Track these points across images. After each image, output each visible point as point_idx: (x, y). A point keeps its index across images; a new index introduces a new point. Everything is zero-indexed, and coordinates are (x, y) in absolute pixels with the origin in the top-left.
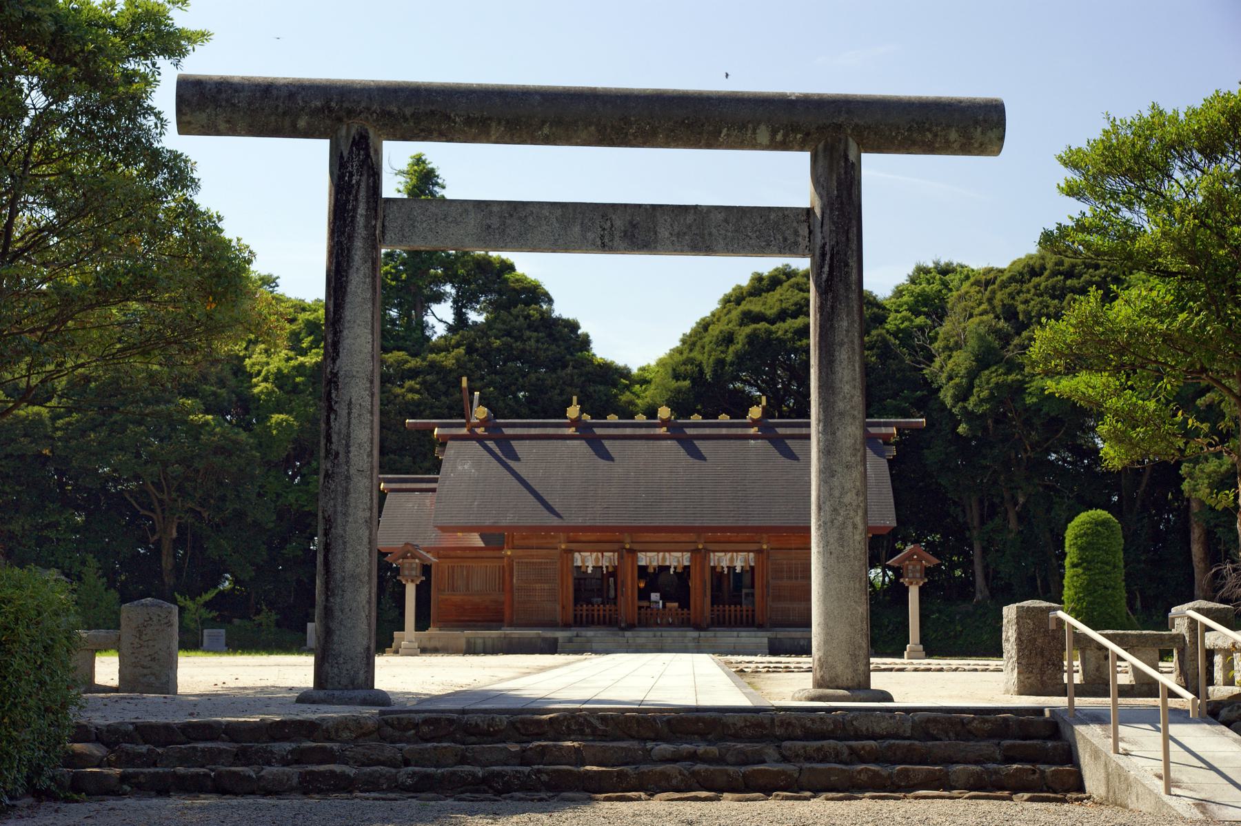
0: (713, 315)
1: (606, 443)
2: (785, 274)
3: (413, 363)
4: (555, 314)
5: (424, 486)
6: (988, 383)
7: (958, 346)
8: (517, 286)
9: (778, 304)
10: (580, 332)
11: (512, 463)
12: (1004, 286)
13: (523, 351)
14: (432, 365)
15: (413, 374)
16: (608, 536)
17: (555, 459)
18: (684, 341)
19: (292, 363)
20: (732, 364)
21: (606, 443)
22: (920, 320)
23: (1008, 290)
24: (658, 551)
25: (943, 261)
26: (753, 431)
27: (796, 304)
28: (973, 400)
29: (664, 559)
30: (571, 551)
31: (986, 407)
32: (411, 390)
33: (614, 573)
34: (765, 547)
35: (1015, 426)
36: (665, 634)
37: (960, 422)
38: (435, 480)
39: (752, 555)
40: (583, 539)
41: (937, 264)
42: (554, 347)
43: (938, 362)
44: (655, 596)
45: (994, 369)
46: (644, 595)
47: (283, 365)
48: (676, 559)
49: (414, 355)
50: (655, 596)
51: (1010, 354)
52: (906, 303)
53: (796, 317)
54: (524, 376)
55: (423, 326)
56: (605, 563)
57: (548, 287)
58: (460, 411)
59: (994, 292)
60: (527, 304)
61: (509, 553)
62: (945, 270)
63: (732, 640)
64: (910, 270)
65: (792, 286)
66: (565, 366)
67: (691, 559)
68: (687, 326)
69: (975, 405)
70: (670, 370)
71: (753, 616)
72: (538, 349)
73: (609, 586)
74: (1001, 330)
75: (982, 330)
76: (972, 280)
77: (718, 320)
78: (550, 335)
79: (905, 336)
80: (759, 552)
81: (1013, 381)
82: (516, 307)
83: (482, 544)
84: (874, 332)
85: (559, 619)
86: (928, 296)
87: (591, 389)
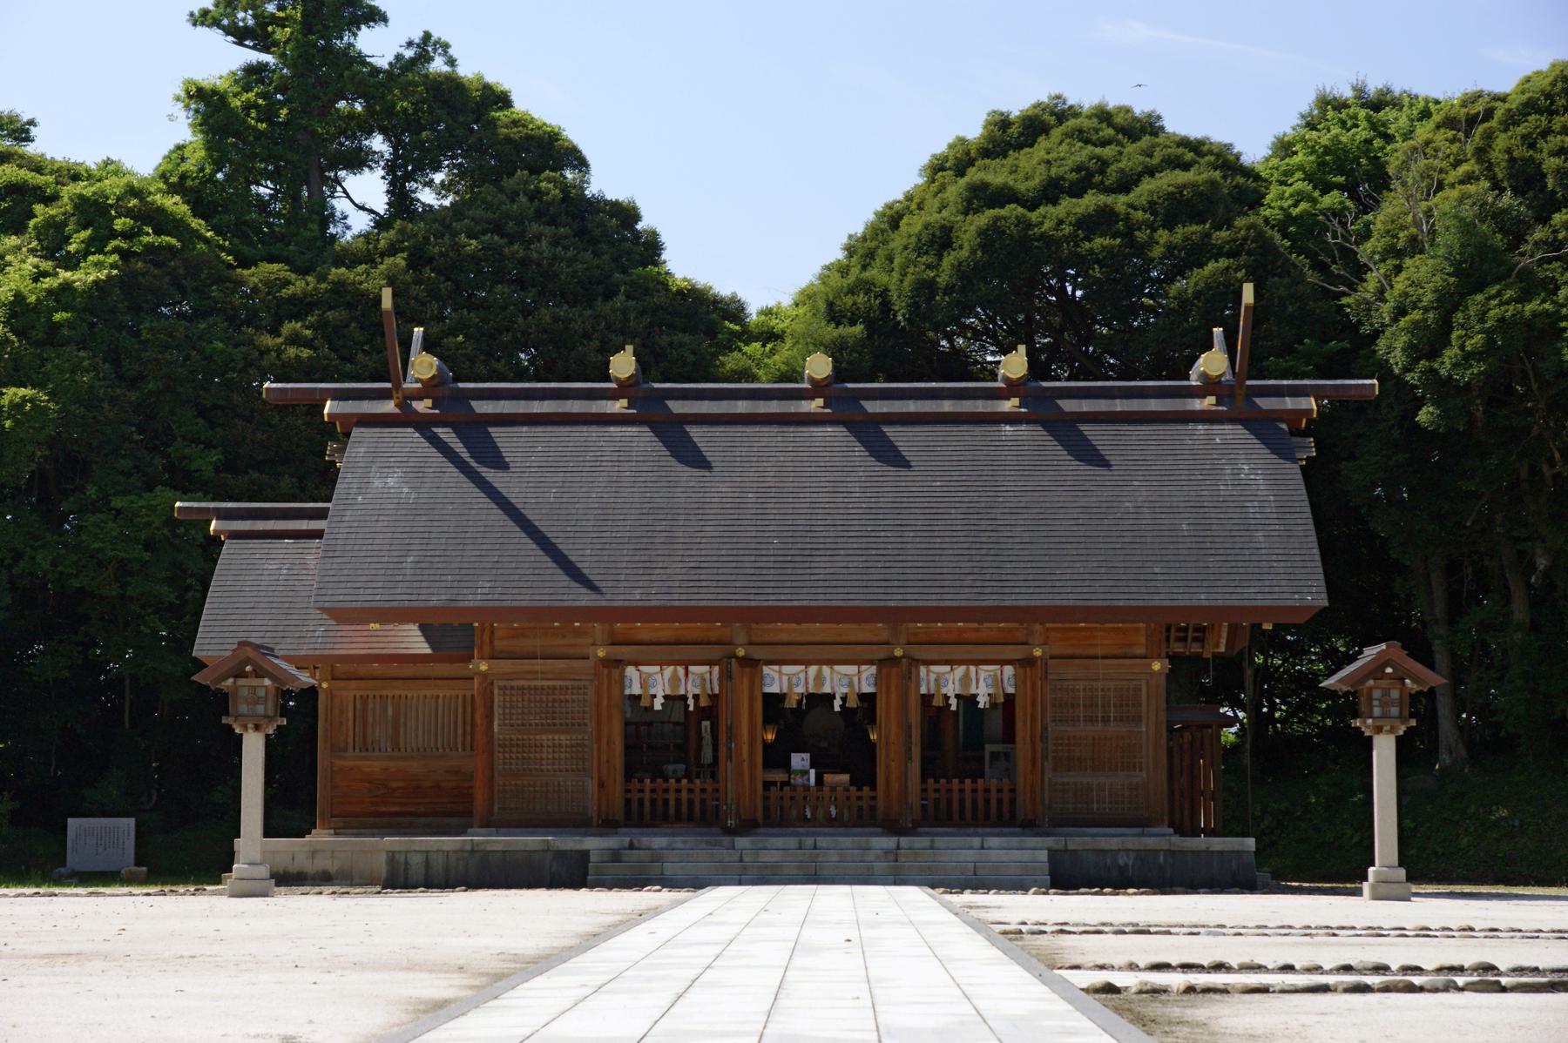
0: (909, 198)
1: (695, 432)
2: (1052, 113)
3: (299, 285)
4: (592, 190)
5: (304, 525)
6: (1482, 320)
7: (1415, 246)
8: (515, 133)
9: (1043, 168)
10: (639, 226)
11: (489, 474)
12: (1511, 121)
13: (524, 262)
14: (340, 287)
15: (299, 307)
16: (697, 629)
17: (584, 467)
18: (850, 250)
19: (47, 283)
20: (949, 290)
21: (695, 432)
22: (1331, 200)
23: (1521, 130)
24: (807, 663)
25: (1373, 86)
26: (1009, 405)
27: (1078, 169)
28: (1450, 354)
29: (819, 679)
30: (620, 664)
31: (1477, 368)
32: (295, 340)
33: (710, 709)
34: (1038, 652)
35: (1530, 412)
36: (823, 842)
37: (1419, 403)
38: (322, 514)
39: (1009, 670)
40: (645, 636)
41: (1360, 91)
42: (588, 255)
43: (1372, 280)
44: (799, 760)
45: (1493, 290)
46: (776, 757)
47: (26, 286)
48: (845, 680)
49: (303, 272)
50: (799, 760)
51: (1525, 262)
52: (1301, 168)
53: (1079, 195)
54: (527, 313)
55: (325, 217)
56: (691, 689)
57: (576, 134)
58: (386, 371)
59: (1489, 136)
60: (536, 171)
61: (483, 667)
62: (1379, 103)
63: (969, 855)
64: (1305, 102)
65: (1068, 135)
66: (609, 295)
67: (878, 679)
68: (858, 221)
69: (1455, 365)
70: (822, 306)
71: (1013, 801)
72: (555, 258)
73: (700, 738)
74: (1504, 211)
75: (1468, 212)
76: (1437, 118)
77: (920, 207)
78: (582, 233)
79: (1304, 230)
80: (1026, 663)
81: (1535, 314)
82: (511, 174)
83: (423, 648)
84: (1240, 222)
85: (592, 810)
86: (1346, 151)
87: (664, 340)
